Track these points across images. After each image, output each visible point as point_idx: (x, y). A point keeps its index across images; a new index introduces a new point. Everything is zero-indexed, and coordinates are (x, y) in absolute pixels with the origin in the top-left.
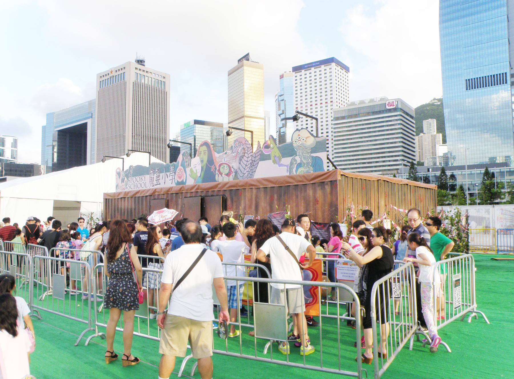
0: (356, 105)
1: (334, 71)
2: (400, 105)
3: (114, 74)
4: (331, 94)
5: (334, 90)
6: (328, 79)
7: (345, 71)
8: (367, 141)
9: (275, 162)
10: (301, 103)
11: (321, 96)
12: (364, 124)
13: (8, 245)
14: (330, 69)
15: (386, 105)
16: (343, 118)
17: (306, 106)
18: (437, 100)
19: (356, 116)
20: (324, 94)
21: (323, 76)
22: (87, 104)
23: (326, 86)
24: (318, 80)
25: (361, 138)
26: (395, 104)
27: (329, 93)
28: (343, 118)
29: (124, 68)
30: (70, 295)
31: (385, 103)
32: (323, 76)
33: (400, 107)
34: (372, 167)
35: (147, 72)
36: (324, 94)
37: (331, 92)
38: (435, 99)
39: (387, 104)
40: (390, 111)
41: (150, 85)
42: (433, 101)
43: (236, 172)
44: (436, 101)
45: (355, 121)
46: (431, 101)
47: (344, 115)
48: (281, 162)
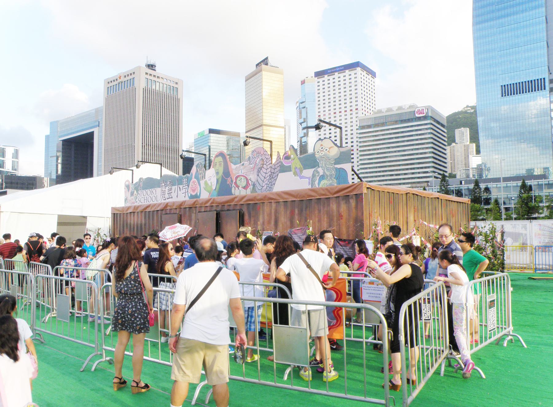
0: (383, 112)
1: (359, 76)
2: (431, 113)
3: (123, 79)
4: (357, 101)
5: (359, 97)
6: (353, 84)
7: (371, 77)
8: (395, 152)
9: (295, 174)
10: (324, 111)
11: (345, 103)
12: (391, 133)
13: (9, 263)
14: (355, 74)
15: (416, 113)
16: (369, 127)
17: (330, 114)
18: (470, 107)
19: (383, 124)
20: (348, 101)
21: (347, 82)
22: (94, 111)
23: (351, 93)
24: (342, 86)
25: (389, 148)
26: (425, 112)
27: (354, 100)
28: (369, 127)
29: (134, 73)
30: (75, 317)
31: (415, 111)
32: (347, 82)
33: (430, 114)
34: (400, 179)
35: (158, 77)
36: (348, 101)
37: (356, 99)
38: (467, 106)
39: (417, 112)
40: (419, 119)
41: (161, 91)
42: (466, 109)
43: (254, 185)
44: (469, 108)
45: (382, 130)
46: (464, 108)
47: (370, 123)
48: (303, 174)
